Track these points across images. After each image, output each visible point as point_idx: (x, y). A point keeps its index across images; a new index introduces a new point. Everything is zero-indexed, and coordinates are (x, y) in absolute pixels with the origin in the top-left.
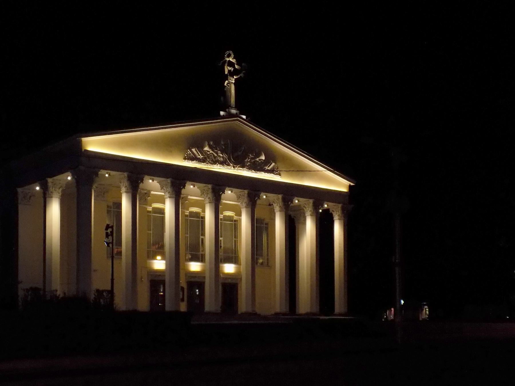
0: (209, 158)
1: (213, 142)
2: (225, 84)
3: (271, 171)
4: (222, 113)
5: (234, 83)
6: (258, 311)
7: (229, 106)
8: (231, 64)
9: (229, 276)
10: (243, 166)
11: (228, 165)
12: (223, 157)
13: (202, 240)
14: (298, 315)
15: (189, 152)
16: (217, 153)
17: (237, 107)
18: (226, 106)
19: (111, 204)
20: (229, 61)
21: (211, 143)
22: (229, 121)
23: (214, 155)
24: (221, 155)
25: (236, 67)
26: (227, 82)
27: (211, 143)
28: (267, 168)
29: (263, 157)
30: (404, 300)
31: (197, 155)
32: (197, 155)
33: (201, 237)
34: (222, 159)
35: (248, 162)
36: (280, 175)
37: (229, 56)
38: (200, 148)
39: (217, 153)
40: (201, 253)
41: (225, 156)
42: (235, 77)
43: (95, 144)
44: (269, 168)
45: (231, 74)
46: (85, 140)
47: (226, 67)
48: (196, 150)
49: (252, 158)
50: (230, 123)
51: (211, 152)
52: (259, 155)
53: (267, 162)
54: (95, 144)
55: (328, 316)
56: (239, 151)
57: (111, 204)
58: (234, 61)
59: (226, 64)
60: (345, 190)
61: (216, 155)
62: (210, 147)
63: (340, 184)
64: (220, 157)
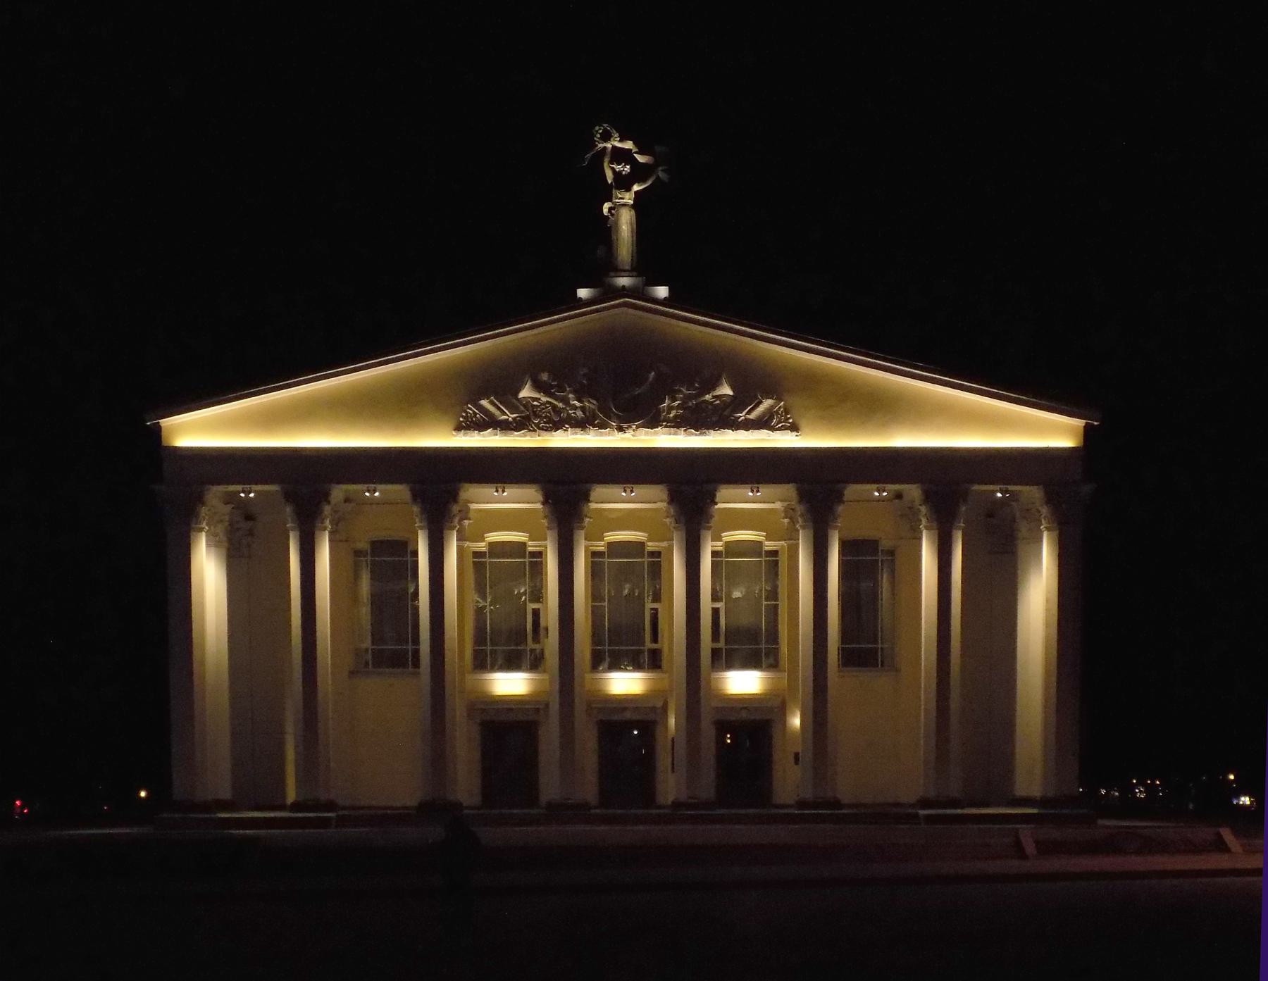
0: (536, 416)
1: (550, 372)
2: (605, 211)
3: (763, 423)
4: (583, 293)
5: (633, 206)
6: (847, 788)
7: (614, 268)
8: (620, 156)
9: (626, 702)
10: (653, 422)
11: (603, 426)
12: (583, 409)
13: (536, 613)
14: (777, 807)
15: (471, 409)
16: (565, 401)
17: (635, 270)
18: (598, 270)
19: (363, 545)
20: (614, 147)
21: (545, 377)
22: (597, 311)
23: (554, 407)
24: (578, 404)
25: (641, 159)
26: (606, 206)
27: (545, 377)
28: (742, 416)
29: (726, 390)
30: (1245, 795)
31: (497, 413)
32: (497, 413)
33: (532, 606)
34: (580, 414)
35: (670, 409)
36: (794, 428)
37: (606, 137)
38: (506, 393)
39: (565, 401)
40: (649, 645)
41: (591, 404)
42: (636, 188)
43: (194, 431)
44: (752, 416)
45: (623, 183)
46: (166, 423)
47: (606, 164)
48: (492, 403)
49: (690, 397)
50: (618, 314)
51: (544, 399)
52: (714, 385)
53: (745, 398)
54: (194, 431)
55: (787, 814)
56: (625, 381)
57: (363, 545)
58: (629, 145)
59: (606, 160)
60: (1066, 442)
61: (561, 405)
62: (538, 386)
63: (1056, 432)
64: (575, 408)
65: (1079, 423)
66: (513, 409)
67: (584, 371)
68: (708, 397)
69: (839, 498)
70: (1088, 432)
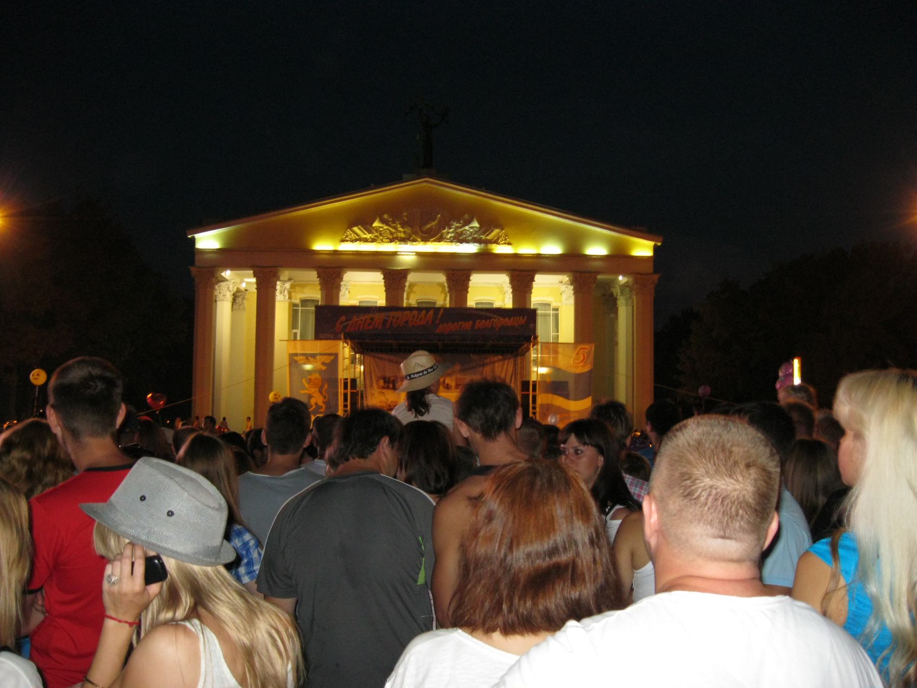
27: (386, 216)
60: (649, 253)
62: (383, 221)
66: (370, 232)
67: (405, 214)
68: (467, 228)
70: (656, 249)
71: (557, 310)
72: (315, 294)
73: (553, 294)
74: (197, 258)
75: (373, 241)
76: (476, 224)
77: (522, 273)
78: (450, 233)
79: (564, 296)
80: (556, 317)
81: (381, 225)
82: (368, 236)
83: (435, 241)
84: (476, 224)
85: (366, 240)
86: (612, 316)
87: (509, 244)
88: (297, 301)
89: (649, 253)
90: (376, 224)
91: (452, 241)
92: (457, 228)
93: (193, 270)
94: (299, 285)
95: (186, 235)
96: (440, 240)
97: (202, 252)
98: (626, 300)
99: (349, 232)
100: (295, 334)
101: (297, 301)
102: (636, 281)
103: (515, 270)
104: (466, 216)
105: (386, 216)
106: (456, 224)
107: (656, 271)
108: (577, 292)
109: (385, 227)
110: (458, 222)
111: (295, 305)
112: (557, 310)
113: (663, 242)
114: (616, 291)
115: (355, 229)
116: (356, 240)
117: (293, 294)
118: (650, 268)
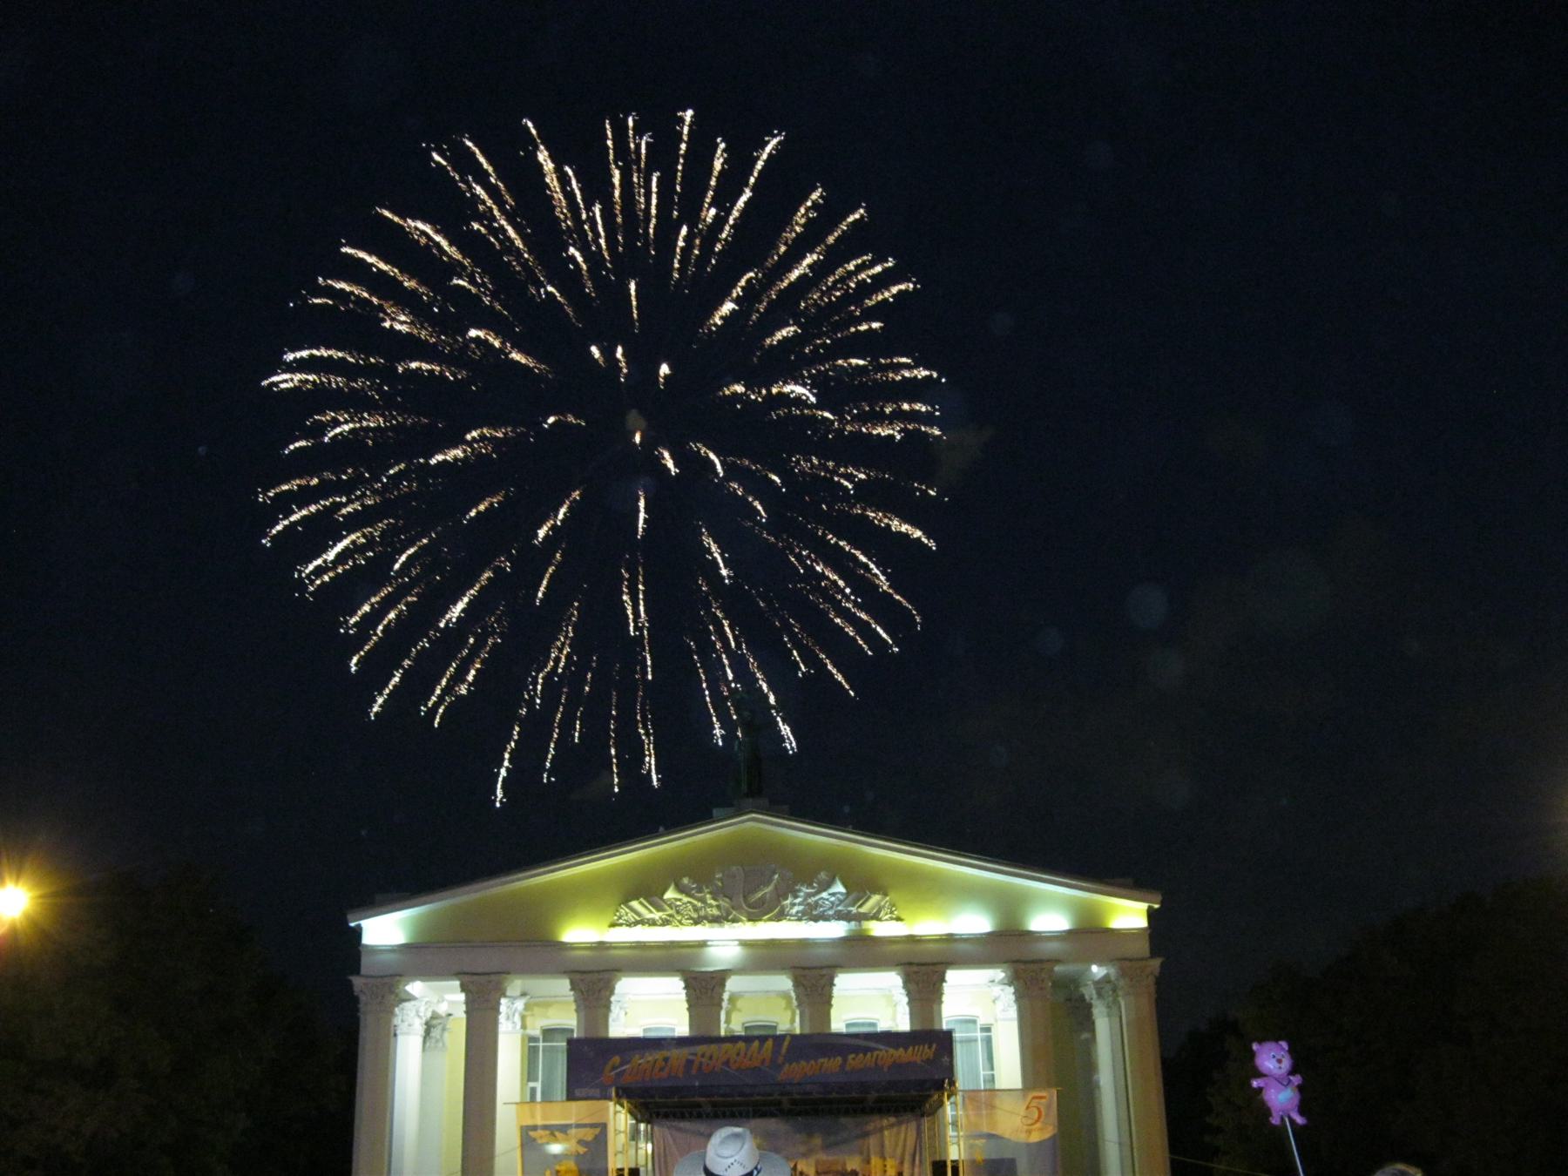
27: (686, 881)
62: (681, 889)
65: (1144, 906)
66: (659, 909)
68: (824, 895)
69: (943, 980)
70: (1151, 914)
71: (987, 1029)
72: (567, 1018)
73: (981, 1004)
74: (365, 961)
75: (665, 923)
76: (839, 888)
77: (924, 971)
78: (794, 904)
79: (1000, 1005)
80: (988, 1042)
81: (678, 896)
82: (657, 915)
83: (770, 919)
84: (839, 888)
85: (653, 923)
86: (1085, 1036)
87: (898, 919)
88: (537, 1033)
89: (1141, 922)
90: (670, 894)
91: (800, 919)
92: (809, 895)
93: (357, 982)
94: (537, 1005)
95: (346, 923)
96: (781, 916)
97: (374, 950)
98: (1109, 1007)
99: (624, 910)
100: (533, 1090)
101: (537, 1033)
102: (1123, 973)
103: (910, 964)
104: (823, 876)
105: (686, 881)
106: (805, 890)
107: (1154, 953)
108: (1020, 997)
109: (686, 899)
110: (810, 885)
111: (532, 1039)
112: (987, 1029)
113: (1162, 903)
114: (1089, 992)
115: (635, 904)
116: (636, 923)
117: (529, 1021)
118: (1143, 947)
